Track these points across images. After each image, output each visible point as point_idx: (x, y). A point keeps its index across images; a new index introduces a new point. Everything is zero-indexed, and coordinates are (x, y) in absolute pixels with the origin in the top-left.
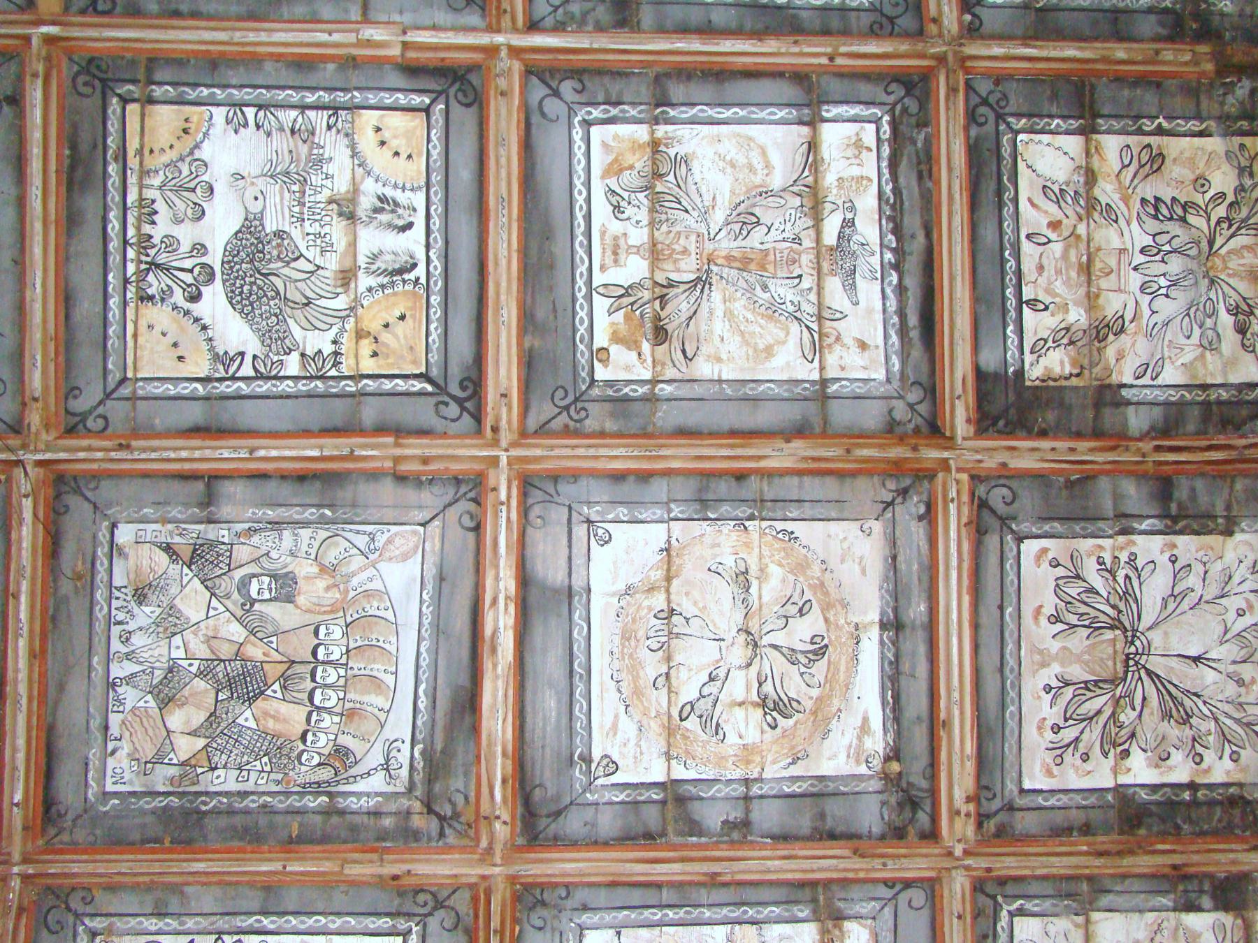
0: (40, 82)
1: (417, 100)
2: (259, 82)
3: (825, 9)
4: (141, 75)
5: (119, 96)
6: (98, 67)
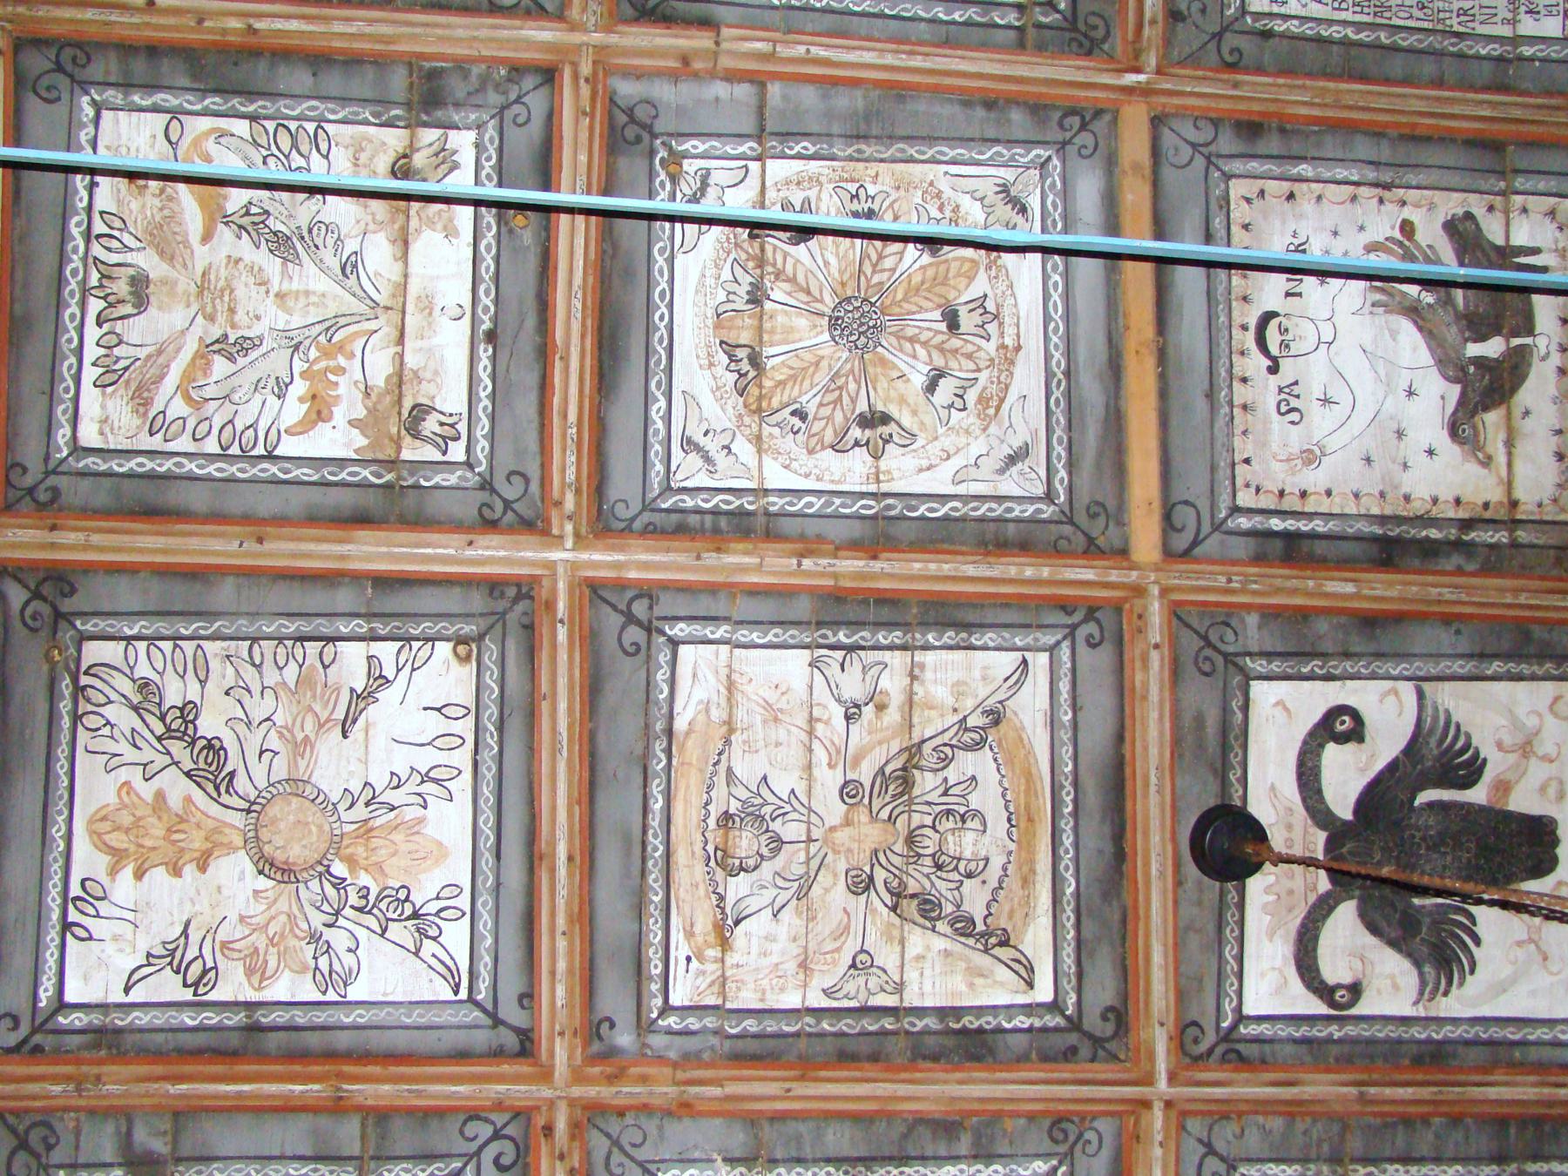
0: (1148, 15)
1: (663, 658)
2: (892, 23)
3: (152, 87)
4: (1031, 33)
5: (1058, 11)
6: (1081, 45)
